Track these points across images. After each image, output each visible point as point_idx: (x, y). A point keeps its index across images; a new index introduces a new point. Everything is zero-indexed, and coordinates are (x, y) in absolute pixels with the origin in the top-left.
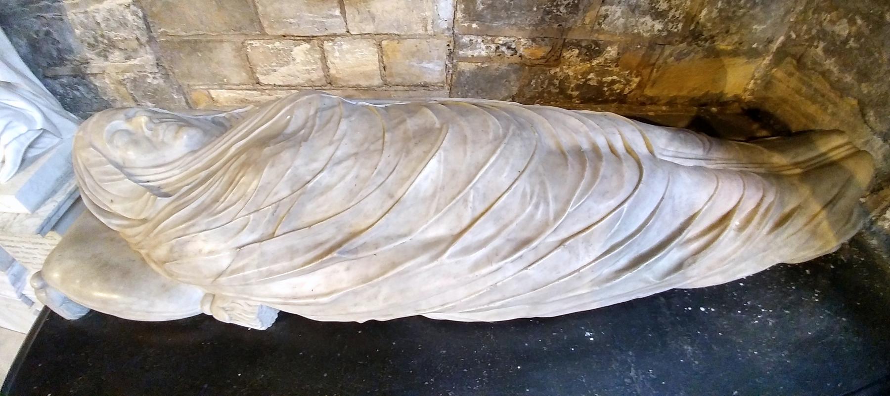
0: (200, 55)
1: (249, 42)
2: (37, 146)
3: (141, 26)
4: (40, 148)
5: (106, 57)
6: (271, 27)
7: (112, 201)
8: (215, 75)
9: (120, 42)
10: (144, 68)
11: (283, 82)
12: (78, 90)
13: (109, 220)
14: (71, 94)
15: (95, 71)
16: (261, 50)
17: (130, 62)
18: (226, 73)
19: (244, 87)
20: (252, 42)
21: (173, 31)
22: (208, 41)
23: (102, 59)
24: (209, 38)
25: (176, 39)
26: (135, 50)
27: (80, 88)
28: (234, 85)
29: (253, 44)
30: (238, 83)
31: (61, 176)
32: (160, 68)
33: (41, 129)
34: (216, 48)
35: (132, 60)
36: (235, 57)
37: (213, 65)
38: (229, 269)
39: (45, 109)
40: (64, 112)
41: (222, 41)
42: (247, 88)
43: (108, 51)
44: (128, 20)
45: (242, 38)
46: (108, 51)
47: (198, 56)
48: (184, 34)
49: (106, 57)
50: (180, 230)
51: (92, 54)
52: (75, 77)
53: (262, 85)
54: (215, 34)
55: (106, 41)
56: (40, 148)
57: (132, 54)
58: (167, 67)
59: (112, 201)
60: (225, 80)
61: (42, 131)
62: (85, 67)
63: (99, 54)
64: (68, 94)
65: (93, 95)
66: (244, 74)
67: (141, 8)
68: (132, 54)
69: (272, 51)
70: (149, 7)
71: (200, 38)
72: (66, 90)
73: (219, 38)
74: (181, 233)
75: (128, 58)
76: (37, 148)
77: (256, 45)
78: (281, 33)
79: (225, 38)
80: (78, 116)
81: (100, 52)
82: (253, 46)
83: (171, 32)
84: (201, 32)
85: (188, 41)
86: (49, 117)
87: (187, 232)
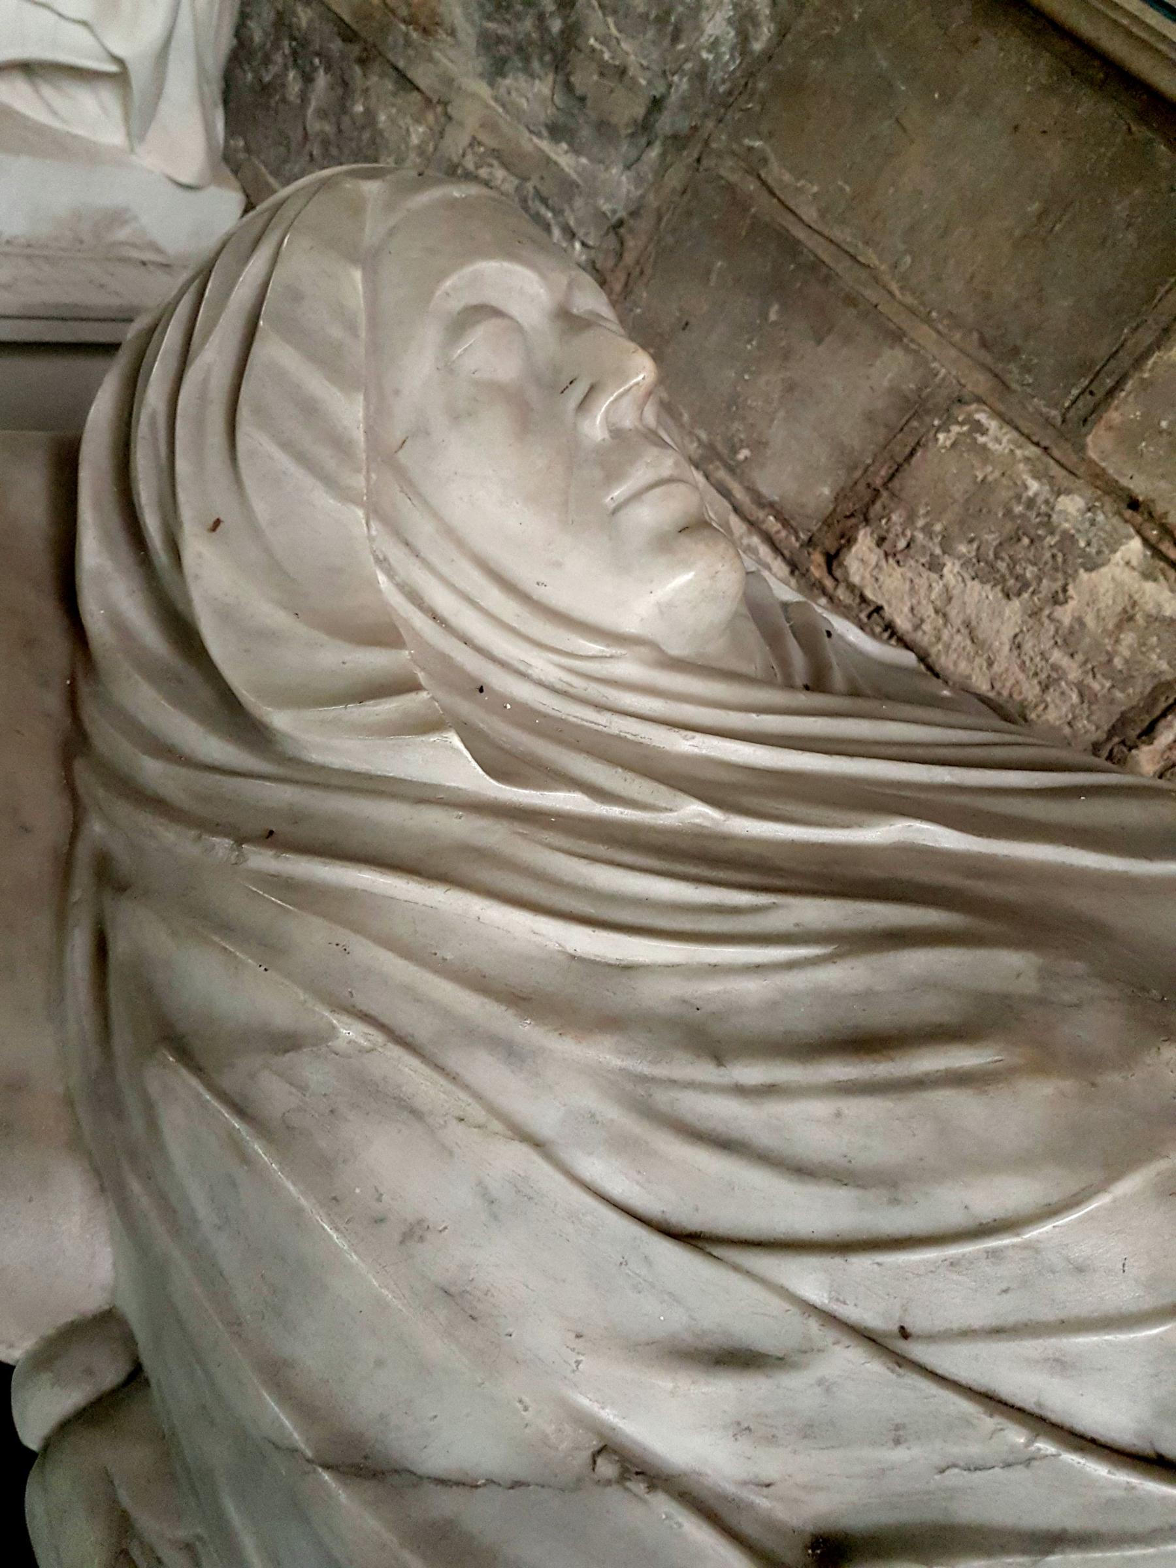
0: (773, 316)
1: (981, 417)
2: (47, 91)
3: (715, 76)
4: (49, 106)
5: (497, 69)
6: (1128, 439)
7: (217, 523)
8: (734, 405)
9: (594, 66)
10: (570, 200)
11: (917, 627)
12: (308, 79)
13: (109, 566)
14: (274, 69)
15: (422, 76)
16: (990, 472)
17: (545, 145)
18: (777, 433)
19: (772, 524)
20: (993, 425)
21: (787, 177)
22: (851, 300)
23: (480, 63)
24: (871, 294)
25: (763, 205)
26: (604, 128)
27: (322, 80)
28: (752, 491)
29: (984, 431)
30: (769, 491)
31: (16, 237)
32: (612, 242)
33: (119, 61)
34: (847, 339)
35: (564, 146)
36: (870, 417)
37: (770, 380)
38: (446, 1504)
39: (185, 26)
40: (214, 90)
41: (897, 337)
42: (776, 538)
43: (527, 60)
44: (699, 29)
45: (979, 382)
46: (527, 60)
47: (764, 316)
48: (810, 213)
49: (497, 69)
50: (445, 1013)
51: (473, 23)
52: (348, 35)
53: (838, 573)
54: (909, 300)
55: (556, 25)
56: (49, 106)
57: (586, 133)
58: (629, 258)
59: (217, 523)
60: (743, 454)
61: (113, 68)
62: (406, 35)
63: (488, 42)
64: (267, 60)
65: (329, 128)
66: (826, 491)
67: (782, 33)
68: (586, 133)
69: (1019, 509)
70: (805, 45)
71: (842, 266)
72: (276, 45)
73: (902, 320)
74: (421, 1026)
75: (556, 132)
76: (41, 97)
77: (992, 446)
78: (1140, 486)
79: (924, 335)
80: (226, 141)
81: (500, 40)
82: (982, 439)
83: (777, 173)
84: (870, 256)
85: (791, 247)
86: (173, 56)
87: (454, 1059)
